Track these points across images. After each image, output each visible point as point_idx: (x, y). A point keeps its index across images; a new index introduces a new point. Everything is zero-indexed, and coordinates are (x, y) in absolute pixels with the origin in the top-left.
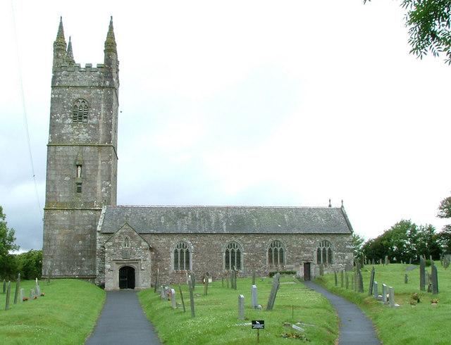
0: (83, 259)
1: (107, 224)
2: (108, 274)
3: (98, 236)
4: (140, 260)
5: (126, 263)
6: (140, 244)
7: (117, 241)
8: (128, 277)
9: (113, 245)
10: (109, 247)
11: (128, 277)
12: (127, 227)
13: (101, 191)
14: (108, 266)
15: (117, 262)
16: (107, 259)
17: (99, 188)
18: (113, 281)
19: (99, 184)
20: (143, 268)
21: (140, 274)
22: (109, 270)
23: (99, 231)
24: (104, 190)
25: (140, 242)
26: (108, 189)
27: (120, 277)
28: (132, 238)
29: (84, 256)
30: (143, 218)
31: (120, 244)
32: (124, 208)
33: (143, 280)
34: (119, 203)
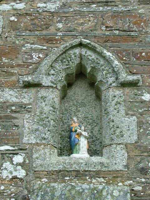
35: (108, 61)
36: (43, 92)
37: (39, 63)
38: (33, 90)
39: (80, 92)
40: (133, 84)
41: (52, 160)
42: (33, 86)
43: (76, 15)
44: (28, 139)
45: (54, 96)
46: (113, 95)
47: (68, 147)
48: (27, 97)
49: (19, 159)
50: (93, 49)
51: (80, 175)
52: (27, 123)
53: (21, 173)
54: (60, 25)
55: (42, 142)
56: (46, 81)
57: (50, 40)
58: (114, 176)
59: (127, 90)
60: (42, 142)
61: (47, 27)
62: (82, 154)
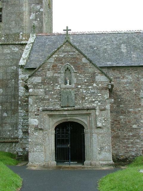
0: (5, 114)
1: (34, 56)
2: (34, 136)
3: (22, 76)
4: (94, 109)
5: (68, 116)
6: (92, 79)
7: (49, 74)
8: (71, 141)
9: (43, 83)
10: (35, 86)
11: (71, 141)
12: (68, 48)
13: (28, 18)
14: (34, 121)
15: (51, 113)
16: (33, 108)
17: (26, 14)
18: (42, 151)
19: (26, 9)
20: (99, 124)
21: (95, 136)
22: (37, 129)
23: (22, 67)
24: (33, 16)
25: (94, 75)
26: (39, 15)
27: (57, 141)
28: (77, 68)
29: (6, 111)
30: (91, 47)
31: (55, 80)
32: (67, 39)
33: (99, 149)
34: (58, 28)
35: (72, 68)
36: (62, 74)
37: (61, 68)
38: (60, 74)
39: (67, 72)
40: (76, 72)
41: (63, 86)
42: (22, 159)
43: (127, 58)
44: (60, 83)
45: (63, 75)
46: (73, 74)
47: (66, 83)
48: (59, 75)
49: (59, 86)
50: (70, 65)
51: (68, 88)
52: (59, 80)
53: (59, 88)
54: (64, 60)
55: (62, 83)
56: (62, 72)
57: (62, 63)
58: (73, 89)
59: (75, 73)
60: (62, 83)
61: (62, 60)
62: (68, 85)
